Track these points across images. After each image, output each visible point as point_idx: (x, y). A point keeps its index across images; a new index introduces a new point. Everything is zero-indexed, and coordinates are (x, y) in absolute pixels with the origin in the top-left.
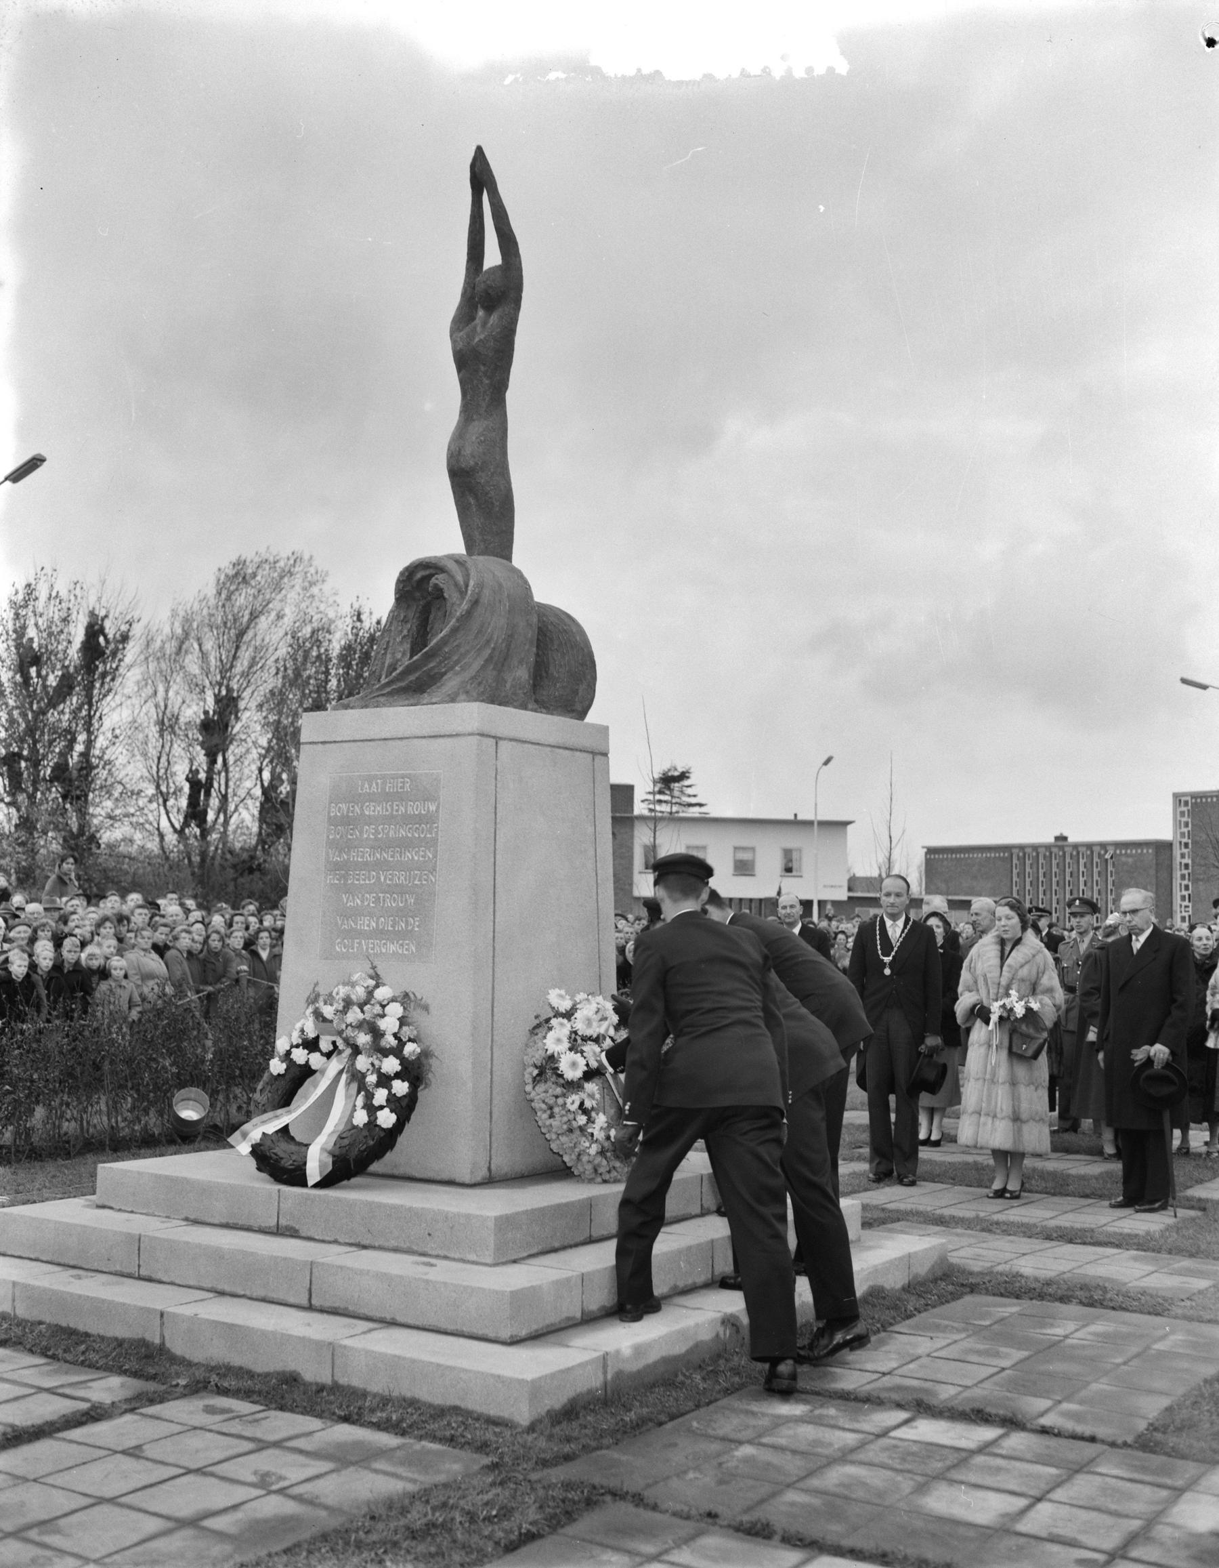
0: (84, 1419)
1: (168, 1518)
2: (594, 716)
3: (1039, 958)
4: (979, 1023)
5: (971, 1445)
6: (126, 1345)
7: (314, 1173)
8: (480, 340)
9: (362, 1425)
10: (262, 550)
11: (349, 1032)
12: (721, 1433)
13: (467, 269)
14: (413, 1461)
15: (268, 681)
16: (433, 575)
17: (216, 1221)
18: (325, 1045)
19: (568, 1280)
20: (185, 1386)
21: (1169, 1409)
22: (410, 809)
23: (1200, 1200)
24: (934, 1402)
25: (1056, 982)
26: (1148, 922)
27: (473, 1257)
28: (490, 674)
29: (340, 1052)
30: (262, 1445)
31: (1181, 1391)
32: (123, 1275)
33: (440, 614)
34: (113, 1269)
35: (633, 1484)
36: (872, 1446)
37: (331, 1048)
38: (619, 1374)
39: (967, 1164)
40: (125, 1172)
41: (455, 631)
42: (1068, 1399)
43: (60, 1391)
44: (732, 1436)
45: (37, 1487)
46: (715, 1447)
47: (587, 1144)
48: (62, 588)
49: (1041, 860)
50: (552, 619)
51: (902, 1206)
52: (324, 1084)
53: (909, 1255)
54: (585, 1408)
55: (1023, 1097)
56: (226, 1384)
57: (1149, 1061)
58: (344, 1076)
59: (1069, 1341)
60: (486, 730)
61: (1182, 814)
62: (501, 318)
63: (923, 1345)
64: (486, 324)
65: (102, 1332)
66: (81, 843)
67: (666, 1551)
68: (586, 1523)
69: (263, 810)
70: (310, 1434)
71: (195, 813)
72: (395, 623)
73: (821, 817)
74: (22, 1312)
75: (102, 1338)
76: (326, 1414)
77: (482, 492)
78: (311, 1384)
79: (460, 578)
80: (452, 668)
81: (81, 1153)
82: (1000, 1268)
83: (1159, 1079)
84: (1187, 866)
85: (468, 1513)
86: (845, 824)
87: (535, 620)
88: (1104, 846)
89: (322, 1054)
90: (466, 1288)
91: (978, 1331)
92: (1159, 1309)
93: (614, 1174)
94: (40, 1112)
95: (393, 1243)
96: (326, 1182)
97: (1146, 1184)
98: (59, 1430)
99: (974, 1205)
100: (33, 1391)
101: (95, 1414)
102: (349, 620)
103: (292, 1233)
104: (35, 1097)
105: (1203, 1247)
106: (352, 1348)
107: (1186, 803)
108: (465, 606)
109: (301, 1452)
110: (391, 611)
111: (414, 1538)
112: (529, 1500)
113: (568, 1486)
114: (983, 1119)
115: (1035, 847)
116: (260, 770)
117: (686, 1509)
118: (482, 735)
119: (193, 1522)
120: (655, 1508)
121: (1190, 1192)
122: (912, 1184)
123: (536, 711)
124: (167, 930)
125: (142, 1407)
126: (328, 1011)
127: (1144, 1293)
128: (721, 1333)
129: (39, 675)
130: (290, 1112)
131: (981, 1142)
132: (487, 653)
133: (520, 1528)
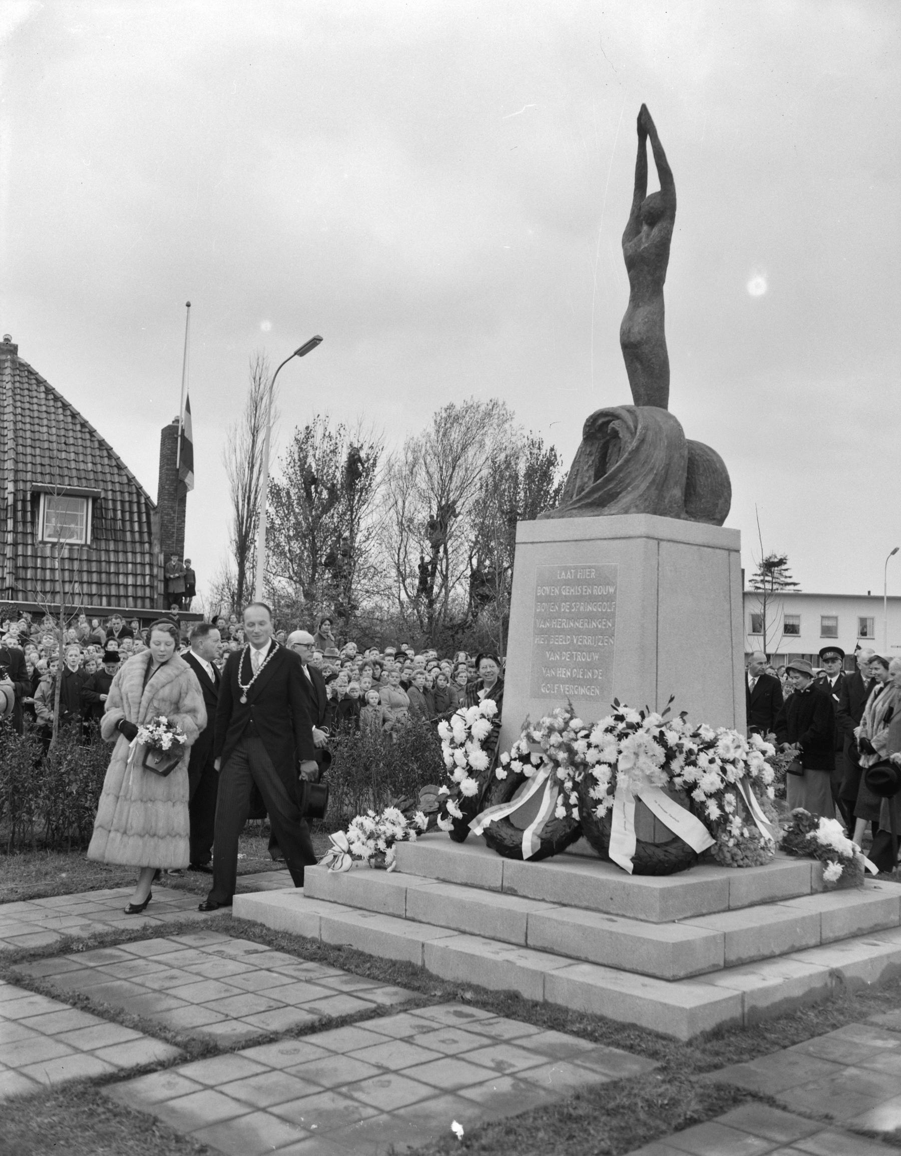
0: (373, 1014)
1: (435, 1087)
2: (729, 523)
4: (122, 739)
6: (397, 965)
7: (527, 848)
8: (645, 248)
9: (566, 1032)
10: (468, 399)
11: (552, 751)
12: (831, 1057)
13: (635, 195)
14: (603, 1060)
16: (609, 422)
17: (459, 882)
18: (534, 759)
19: (714, 937)
20: (440, 997)
22: (595, 591)
27: (642, 917)
28: (653, 492)
29: (546, 765)
30: (496, 1041)
32: (394, 916)
34: (387, 911)
35: (768, 1089)
37: (539, 761)
38: (753, 1009)
41: (627, 461)
43: (355, 994)
44: (841, 1060)
45: (344, 1059)
46: (828, 1067)
47: (726, 839)
50: (698, 451)
52: (533, 788)
54: (728, 1031)
58: (549, 782)
60: (651, 534)
62: (660, 231)
64: (649, 236)
65: (381, 955)
66: (346, 611)
67: (795, 1141)
68: (735, 1114)
69: (472, 586)
70: (529, 1036)
71: (425, 588)
72: (583, 456)
73: (891, 593)
74: (327, 938)
75: (382, 959)
76: (540, 1023)
78: (528, 1001)
80: (626, 488)
85: (647, 1101)
87: (686, 453)
89: (533, 766)
90: (639, 938)
95: (585, 904)
96: (537, 857)
98: (356, 1021)
100: (336, 993)
101: (379, 1012)
103: (512, 892)
106: (557, 977)
108: (635, 444)
109: (524, 1048)
110: (580, 448)
111: (609, 1115)
112: (691, 1095)
113: (719, 1087)
114: (112, 834)
116: (471, 558)
117: (808, 1111)
118: (648, 537)
119: (453, 1091)
120: (784, 1108)
123: (686, 519)
125: (411, 1009)
126: (537, 735)
128: (829, 984)
129: (316, 491)
130: (510, 806)
132: (650, 478)
133: (685, 1115)
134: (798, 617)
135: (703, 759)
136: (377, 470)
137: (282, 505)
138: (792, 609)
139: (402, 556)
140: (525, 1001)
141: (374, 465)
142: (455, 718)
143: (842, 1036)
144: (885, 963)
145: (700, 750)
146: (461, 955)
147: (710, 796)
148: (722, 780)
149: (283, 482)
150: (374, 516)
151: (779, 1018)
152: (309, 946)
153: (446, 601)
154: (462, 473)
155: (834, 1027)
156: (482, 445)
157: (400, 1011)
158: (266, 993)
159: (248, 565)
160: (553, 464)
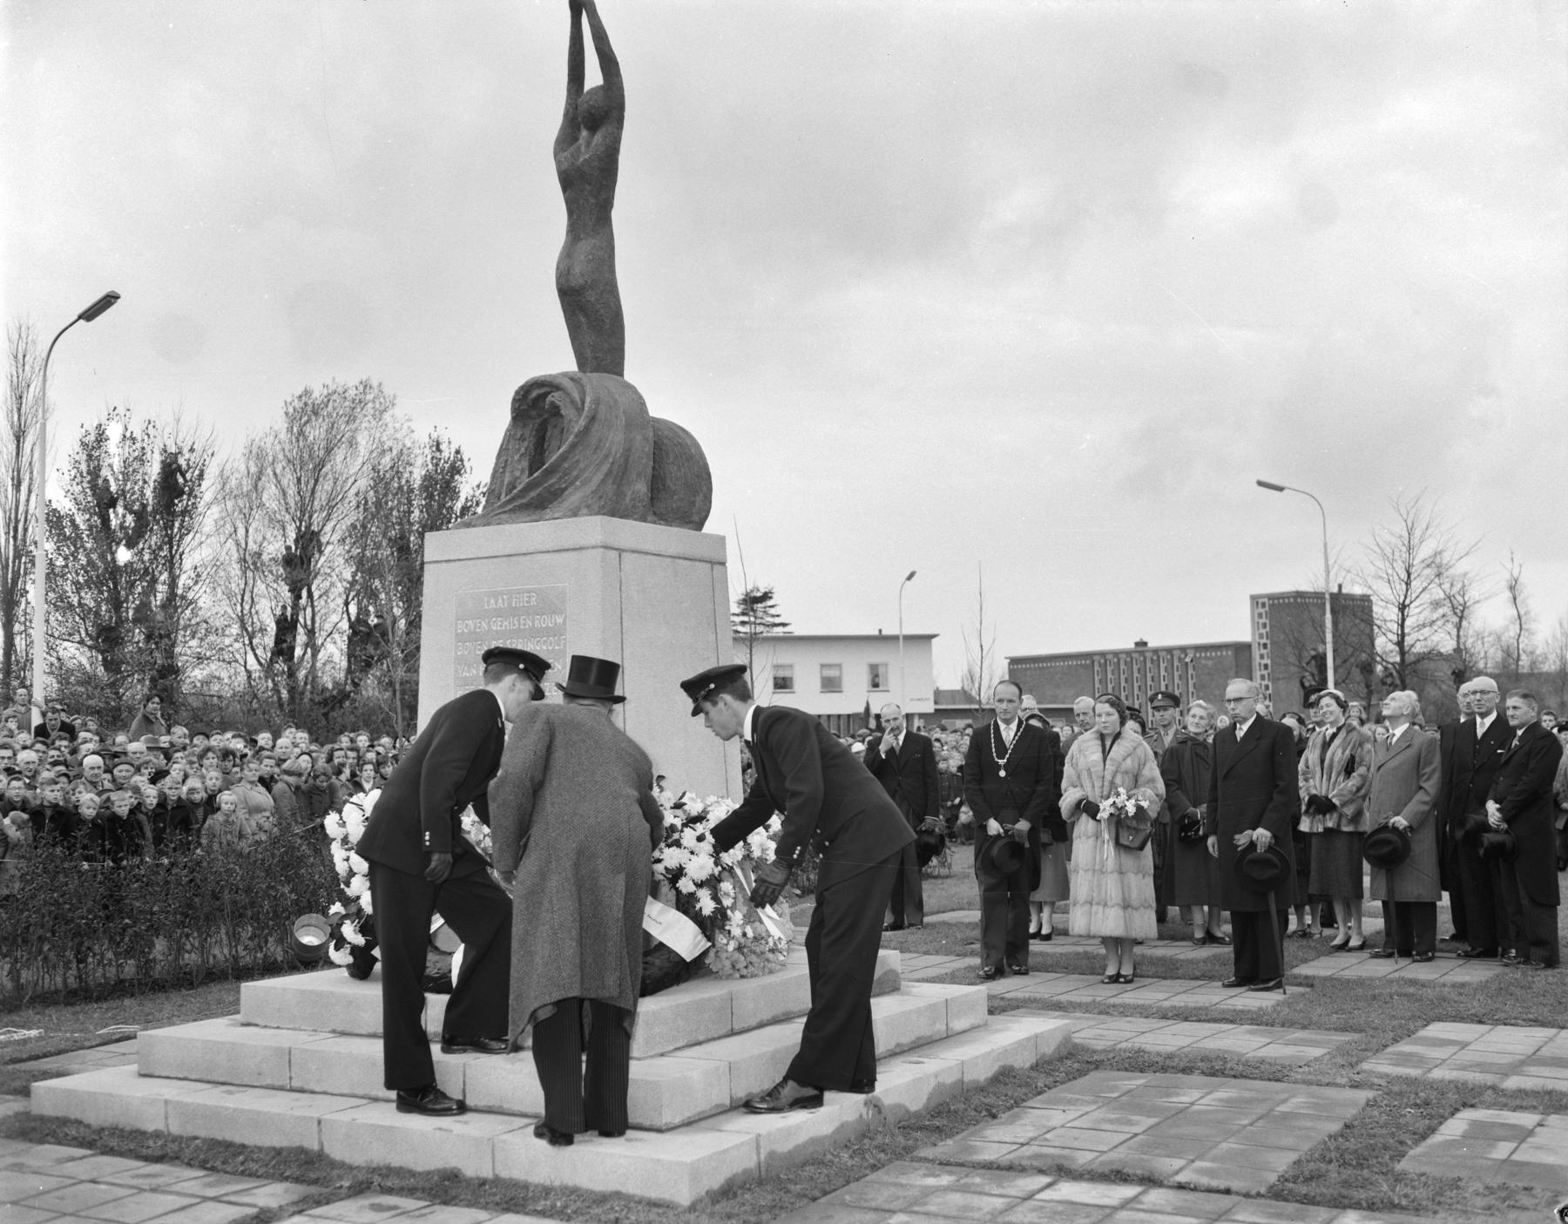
3: (1139, 751)
5: (1114, 1202)
9: (527, 1214)
10: (329, 382)
12: (873, 1204)
15: (346, 515)
16: (545, 395)
21: (1298, 1163)
23: (1307, 977)
24: (1073, 1167)
25: (1157, 773)
26: (1251, 711)
28: (610, 488)
31: (1306, 1147)
32: (274, 1088)
33: (556, 432)
36: (1019, 1209)
38: (772, 1154)
39: (1078, 954)
40: (50, 1089)
41: (573, 447)
42: (1201, 1157)
44: (887, 1207)
48: (137, 429)
49: (1122, 666)
51: (1020, 995)
53: (1036, 1036)
54: (741, 1187)
55: (1133, 885)
56: (389, 1184)
57: (1252, 845)
59: (1195, 1108)
61: (1260, 616)
63: (1056, 1117)
64: (589, 145)
71: (283, 648)
73: (908, 631)
74: (175, 1129)
75: (260, 1149)
77: (591, 307)
79: (576, 396)
80: (572, 483)
81: (203, 983)
82: (1123, 1045)
83: (1263, 862)
84: (1266, 666)
86: (929, 638)
88: (1183, 649)
91: (1108, 1102)
92: (1280, 1075)
93: (751, 969)
94: (160, 945)
97: (1257, 965)
99: (1090, 991)
102: (427, 451)
104: (155, 929)
105: (1315, 1019)
107: (1264, 605)
108: (582, 422)
114: (1094, 908)
115: (1116, 654)
116: (347, 604)
118: (606, 547)
121: (1296, 971)
122: (1026, 973)
124: (272, 762)
127: (1262, 1061)
131: (1094, 931)
132: (605, 468)
134: (791, 666)
135: (689, 836)
136: (205, 484)
137: (67, 538)
138: (785, 656)
139: (247, 607)
140: (468, 1182)
141: (201, 476)
142: (347, 808)
143: (885, 1178)
144: (933, 1083)
145: (685, 825)
146: (374, 1128)
147: (700, 885)
148: (716, 864)
149: (64, 505)
150: (204, 547)
151: (804, 1164)
152: (151, 1143)
153: (313, 665)
154: (328, 486)
155: (874, 1168)
156: (352, 443)
157: (294, 1214)
158: (92, 1213)
159: (17, 627)
160: (458, 472)
